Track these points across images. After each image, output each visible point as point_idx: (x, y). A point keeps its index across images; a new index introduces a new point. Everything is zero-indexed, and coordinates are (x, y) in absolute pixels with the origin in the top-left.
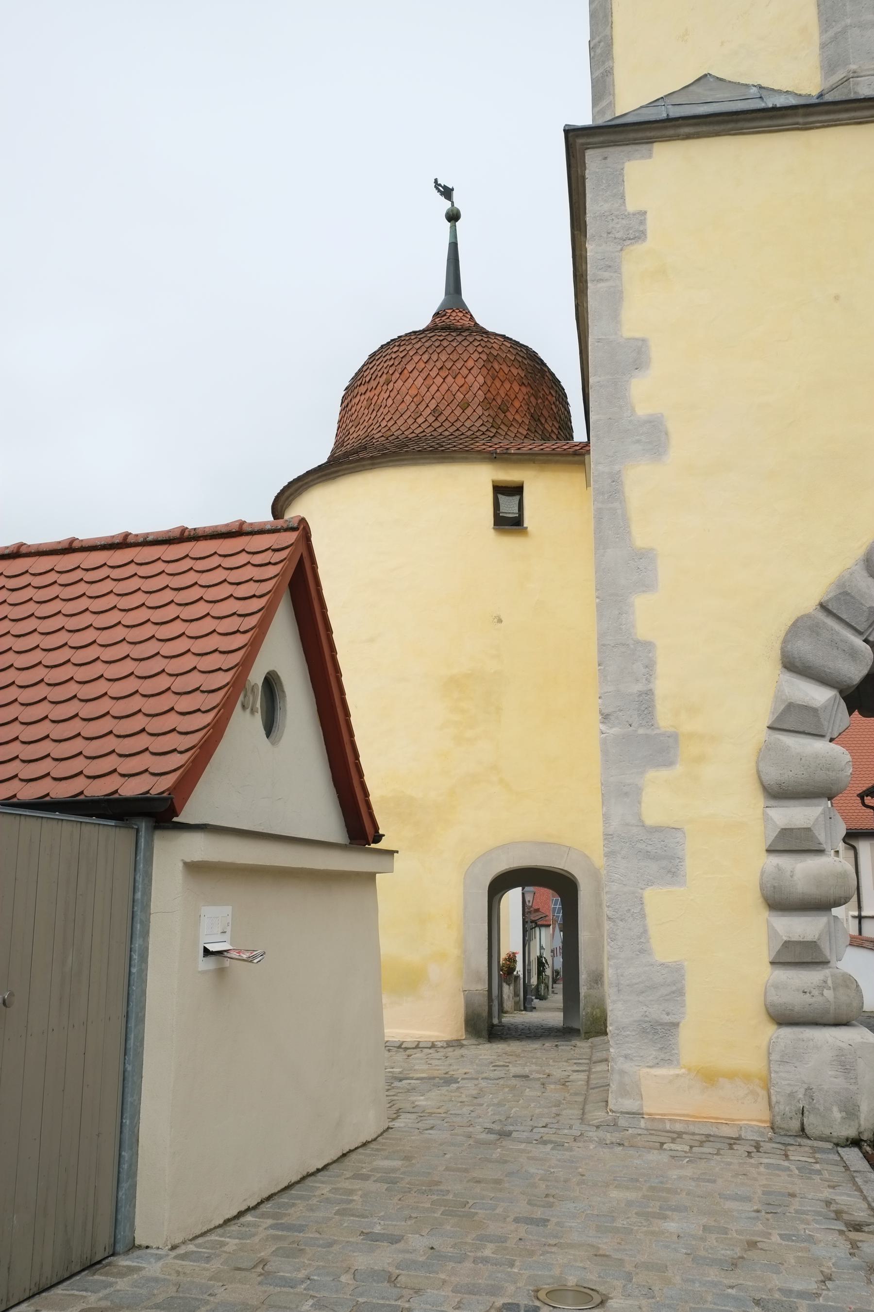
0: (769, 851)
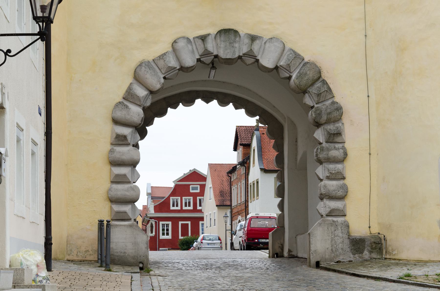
0: (112, 182)
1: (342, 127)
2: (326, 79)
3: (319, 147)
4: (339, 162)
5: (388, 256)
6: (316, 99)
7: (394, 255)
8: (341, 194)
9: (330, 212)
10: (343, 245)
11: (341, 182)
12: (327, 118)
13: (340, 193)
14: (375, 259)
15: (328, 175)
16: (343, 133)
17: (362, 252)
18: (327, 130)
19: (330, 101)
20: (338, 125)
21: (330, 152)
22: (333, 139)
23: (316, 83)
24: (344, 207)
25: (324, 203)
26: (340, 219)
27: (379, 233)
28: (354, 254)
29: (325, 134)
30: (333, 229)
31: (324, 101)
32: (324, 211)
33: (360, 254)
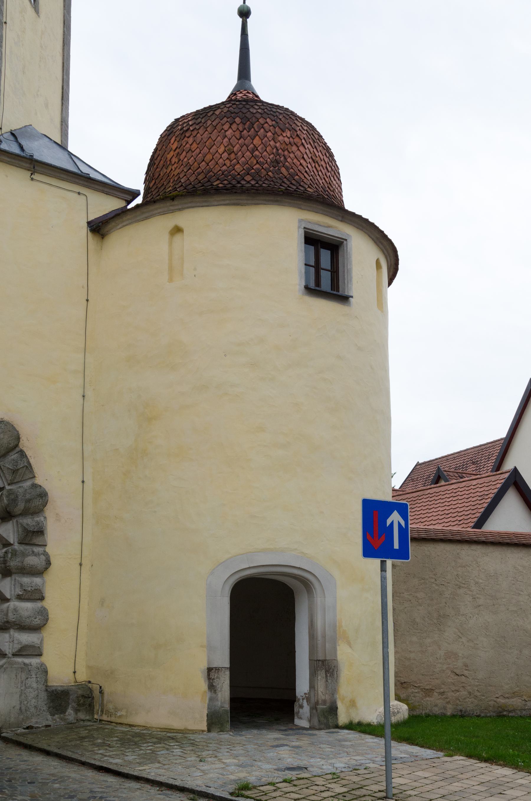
1: (45, 523)
2: (24, 449)
3: (10, 550)
4: (37, 574)
5: (105, 718)
6: (9, 478)
7: (120, 717)
8: (39, 622)
9: (20, 650)
10: (37, 700)
11: (39, 604)
12: (25, 507)
13: (37, 621)
14: (83, 720)
15: (21, 593)
16: (45, 532)
17: (64, 712)
18: (22, 525)
19: (28, 483)
20: (38, 519)
21: (26, 559)
22: (31, 540)
23: (11, 454)
24: (41, 643)
25: (10, 635)
26: (34, 661)
27: (90, 682)
28: (52, 715)
29: (18, 531)
30: (24, 676)
31: (21, 481)
32: (8, 649)
33: (61, 713)
